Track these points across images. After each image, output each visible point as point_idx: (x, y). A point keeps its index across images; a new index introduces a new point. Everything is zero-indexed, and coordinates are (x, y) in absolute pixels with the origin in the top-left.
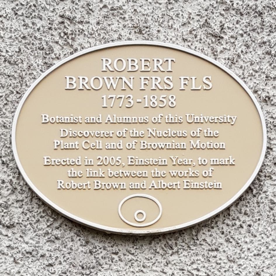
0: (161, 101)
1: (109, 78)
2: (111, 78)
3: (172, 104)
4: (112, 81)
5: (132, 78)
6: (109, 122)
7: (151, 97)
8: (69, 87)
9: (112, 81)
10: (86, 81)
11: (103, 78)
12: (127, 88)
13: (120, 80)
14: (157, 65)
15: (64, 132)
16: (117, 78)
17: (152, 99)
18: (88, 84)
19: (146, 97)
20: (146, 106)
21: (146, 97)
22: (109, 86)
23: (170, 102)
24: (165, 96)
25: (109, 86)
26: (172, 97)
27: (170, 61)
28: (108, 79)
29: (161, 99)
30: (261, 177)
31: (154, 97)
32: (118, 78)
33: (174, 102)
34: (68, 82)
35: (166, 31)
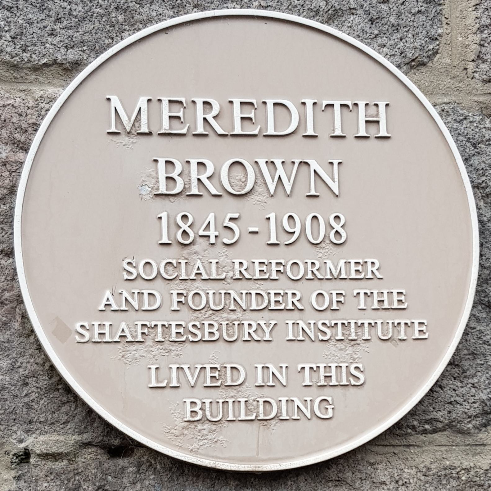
0: (226, 227)
1: (272, 162)
2: (278, 163)
3: (338, 236)
4: (280, 171)
5: (336, 162)
6: (282, 277)
7: (179, 218)
8: (166, 191)
9: (280, 171)
10: (209, 172)
11: (256, 162)
12: (322, 191)
13: (304, 167)
14: (199, 177)
15: (152, 297)
16: (293, 163)
17: (180, 223)
18: (215, 180)
19: (164, 215)
20: (165, 240)
21: (272, 216)
22: (272, 187)
23: (334, 231)
24: (236, 215)
25: (272, 187)
26: (337, 217)
27: (337, 108)
28: (271, 166)
29: (227, 223)
30: (457, 426)
31: (185, 217)
32: (297, 162)
33: (341, 231)
34: (162, 176)
35: (64, 12)
